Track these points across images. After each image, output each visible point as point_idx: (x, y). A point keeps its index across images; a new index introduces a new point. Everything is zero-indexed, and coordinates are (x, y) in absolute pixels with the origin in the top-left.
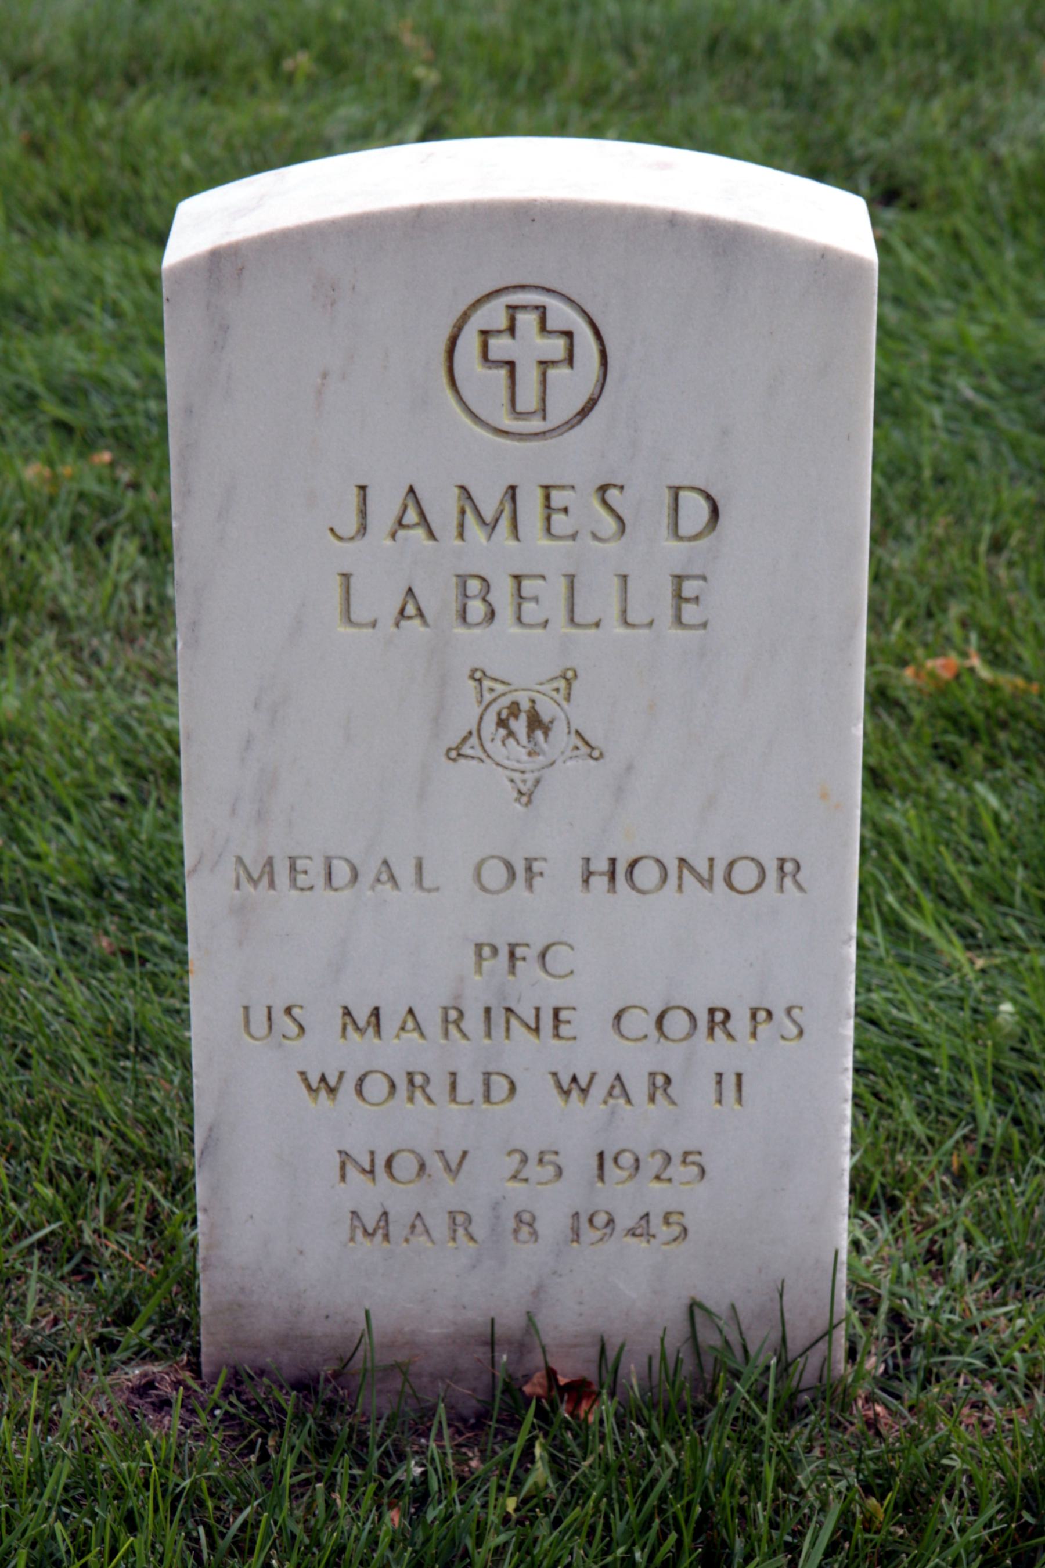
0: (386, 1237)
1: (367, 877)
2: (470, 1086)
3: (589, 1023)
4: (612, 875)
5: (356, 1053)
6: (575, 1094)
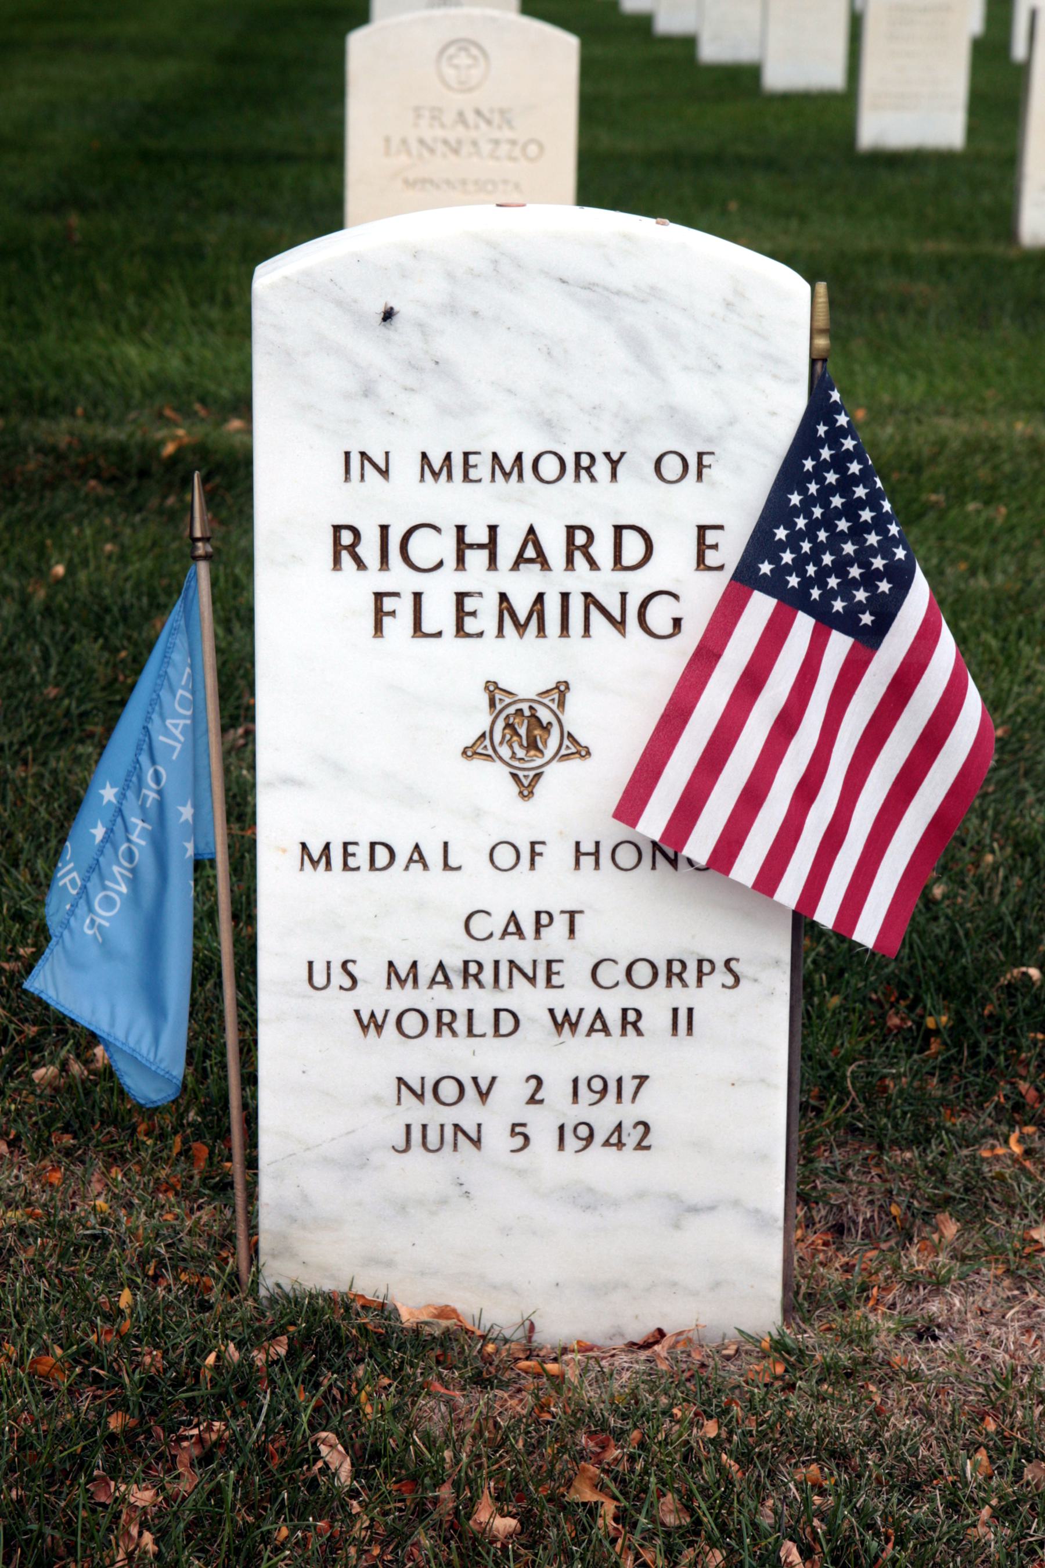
0: (450, 476)
1: (402, 858)
2: (483, 1023)
4: (596, 854)
5: (400, 998)
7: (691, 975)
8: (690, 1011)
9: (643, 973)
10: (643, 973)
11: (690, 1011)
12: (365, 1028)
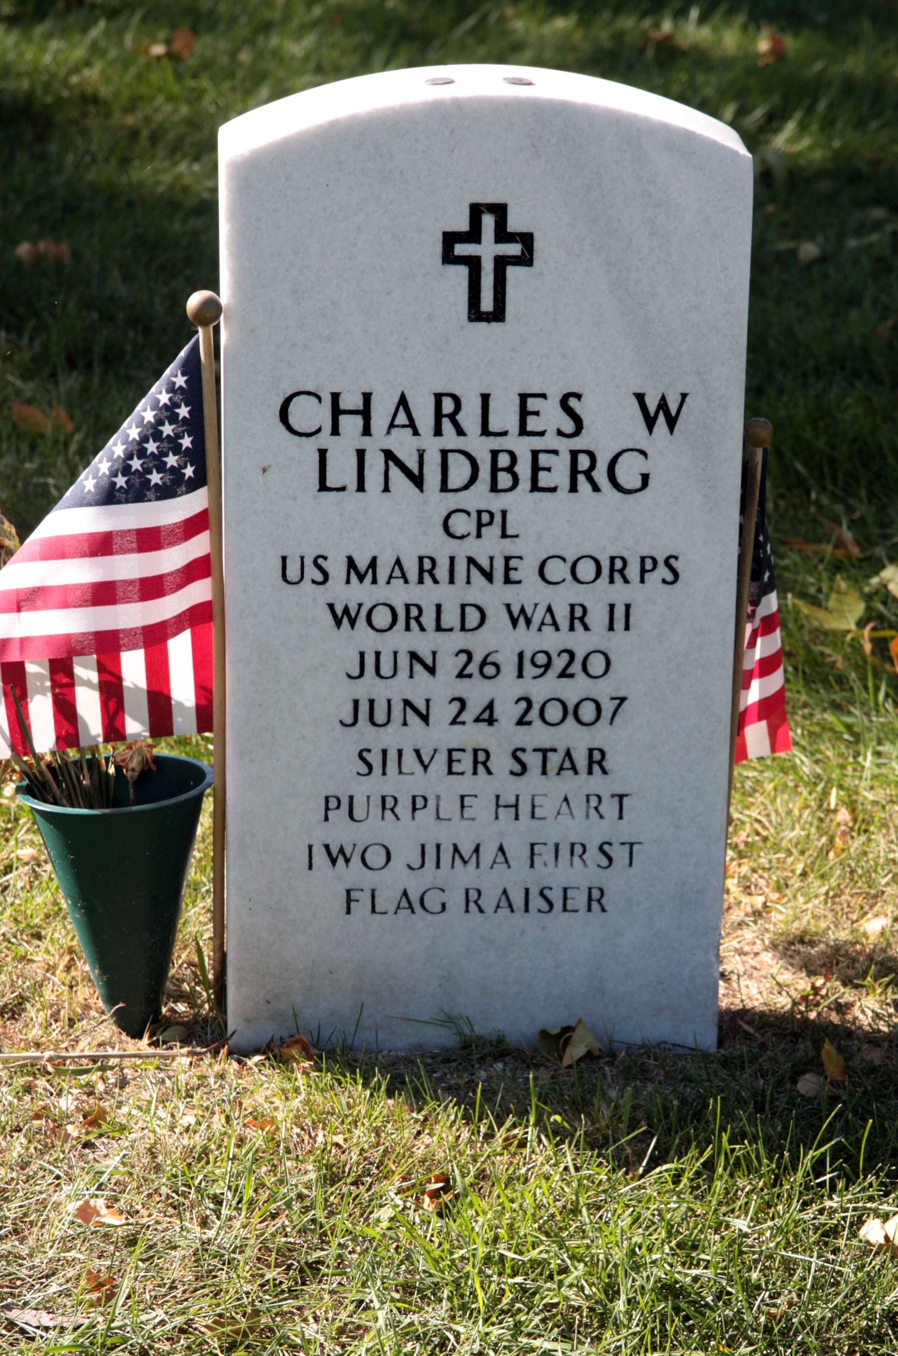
3: (526, 571)
6: (341, 861)
7: (633, 571)
8: (628, 607)
9: (586, 570)
10: (586, 570)
11: (628, 607)
12: (338, 622)
